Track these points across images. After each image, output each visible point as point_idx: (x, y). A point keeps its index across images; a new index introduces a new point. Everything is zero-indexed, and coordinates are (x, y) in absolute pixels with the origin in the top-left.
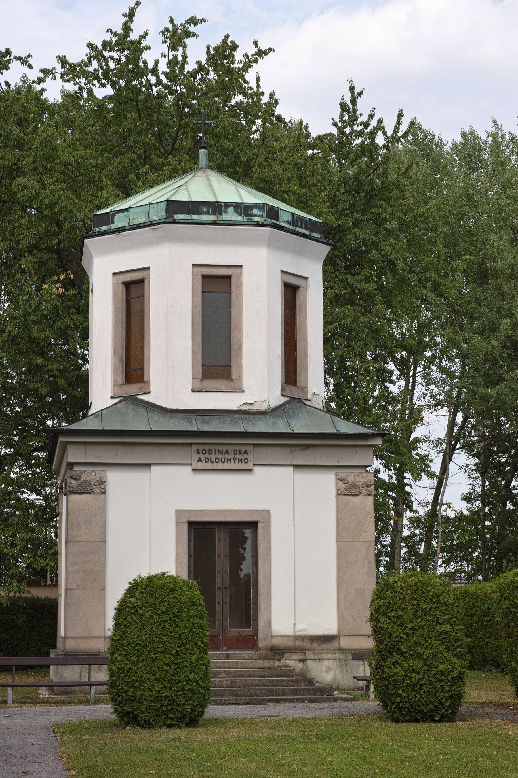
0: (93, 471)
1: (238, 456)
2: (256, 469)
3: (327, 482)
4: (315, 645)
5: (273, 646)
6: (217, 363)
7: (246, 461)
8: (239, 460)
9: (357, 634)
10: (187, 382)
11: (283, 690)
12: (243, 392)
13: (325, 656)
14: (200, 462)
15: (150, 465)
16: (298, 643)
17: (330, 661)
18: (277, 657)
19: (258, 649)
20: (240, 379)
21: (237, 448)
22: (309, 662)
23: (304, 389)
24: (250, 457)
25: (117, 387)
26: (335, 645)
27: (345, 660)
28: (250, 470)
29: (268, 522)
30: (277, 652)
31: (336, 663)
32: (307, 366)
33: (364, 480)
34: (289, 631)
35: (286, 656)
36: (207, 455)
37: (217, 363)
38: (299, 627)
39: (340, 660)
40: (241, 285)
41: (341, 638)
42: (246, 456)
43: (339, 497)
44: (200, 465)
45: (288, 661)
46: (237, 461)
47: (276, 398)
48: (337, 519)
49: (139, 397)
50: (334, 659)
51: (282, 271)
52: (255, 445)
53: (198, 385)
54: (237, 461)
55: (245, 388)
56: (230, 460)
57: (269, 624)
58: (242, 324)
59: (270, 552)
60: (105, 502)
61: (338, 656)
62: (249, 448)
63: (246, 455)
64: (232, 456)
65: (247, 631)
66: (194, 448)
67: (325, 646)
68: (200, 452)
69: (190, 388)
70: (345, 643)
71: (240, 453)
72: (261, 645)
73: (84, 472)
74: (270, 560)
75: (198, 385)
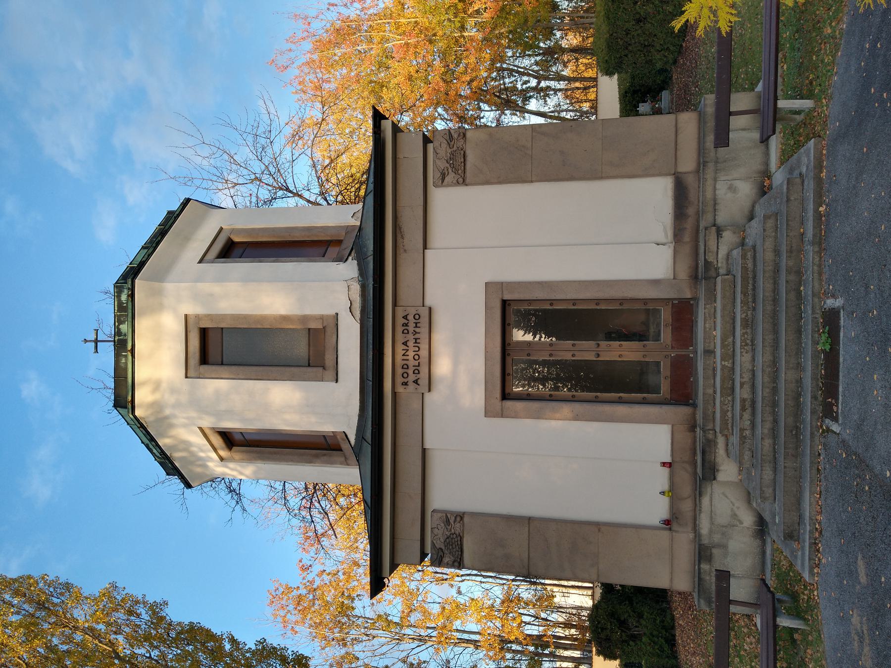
0: (432, 532)
1: (411, 328)
2: (428, 303)
3: (445, 199)
4: (691, 211)
5: (691, 276)
6: (299, 351)
7: (417, 317)
8: (416, 327)
9: (673, 144)
10: (328, 386)
11: (789, 271)
12: (337, 314)
13: (709, 195)
14: (419, 382)
15: (424, 451)
16: (687, 238)
17: (718, 186)
18: (712, 273)
19: (696, 299)
20: (322, 318)
21: (399, 329)
22: (721, 219)
23: (348, 229)
24: (412, 312)
25: (349, 462)
26: (690, 180)
27: (716, 162)
28: (430, 309)
29: (501, 285)
30: (701, 272)
31: (722, 177)
32: (322, 227)
33: (445, 145)
34: (667, 253)
35: (711, 258)
36: (410, 372)
37: (299, 351)
38: (661, 238)
39: (716, 171)
40: (209, 315)
41: (680, 170)
42: (410, 317)
43: (468, 181)
44: (424, 381)
45: (720, 256)
46: (417, 330)
47: (349, 269)
48: (500, 183)
49: (353, 441)
50: (715, 180)
51: (200, 262)
52: (395, 304)
53: (330, 373)
54: (417, 330)
55: (333, 312)
56: (416, 339)
57: (656, 282)
58: (256, 315)
59: (546, 282)
60: (474, 515)
61: (710, 173)
62: (400, 312)
63: (409, 317)
64: (411, 337)
65: (666, 315)
66: (400, 389)
67: (692, 195)
68: (406, 380)
69: (334, 384)
70: (687, 164)
71: (407, 325)
72: (688, 295)
73: (433, 544)
74: (558, 282)
75: (330, 373)
